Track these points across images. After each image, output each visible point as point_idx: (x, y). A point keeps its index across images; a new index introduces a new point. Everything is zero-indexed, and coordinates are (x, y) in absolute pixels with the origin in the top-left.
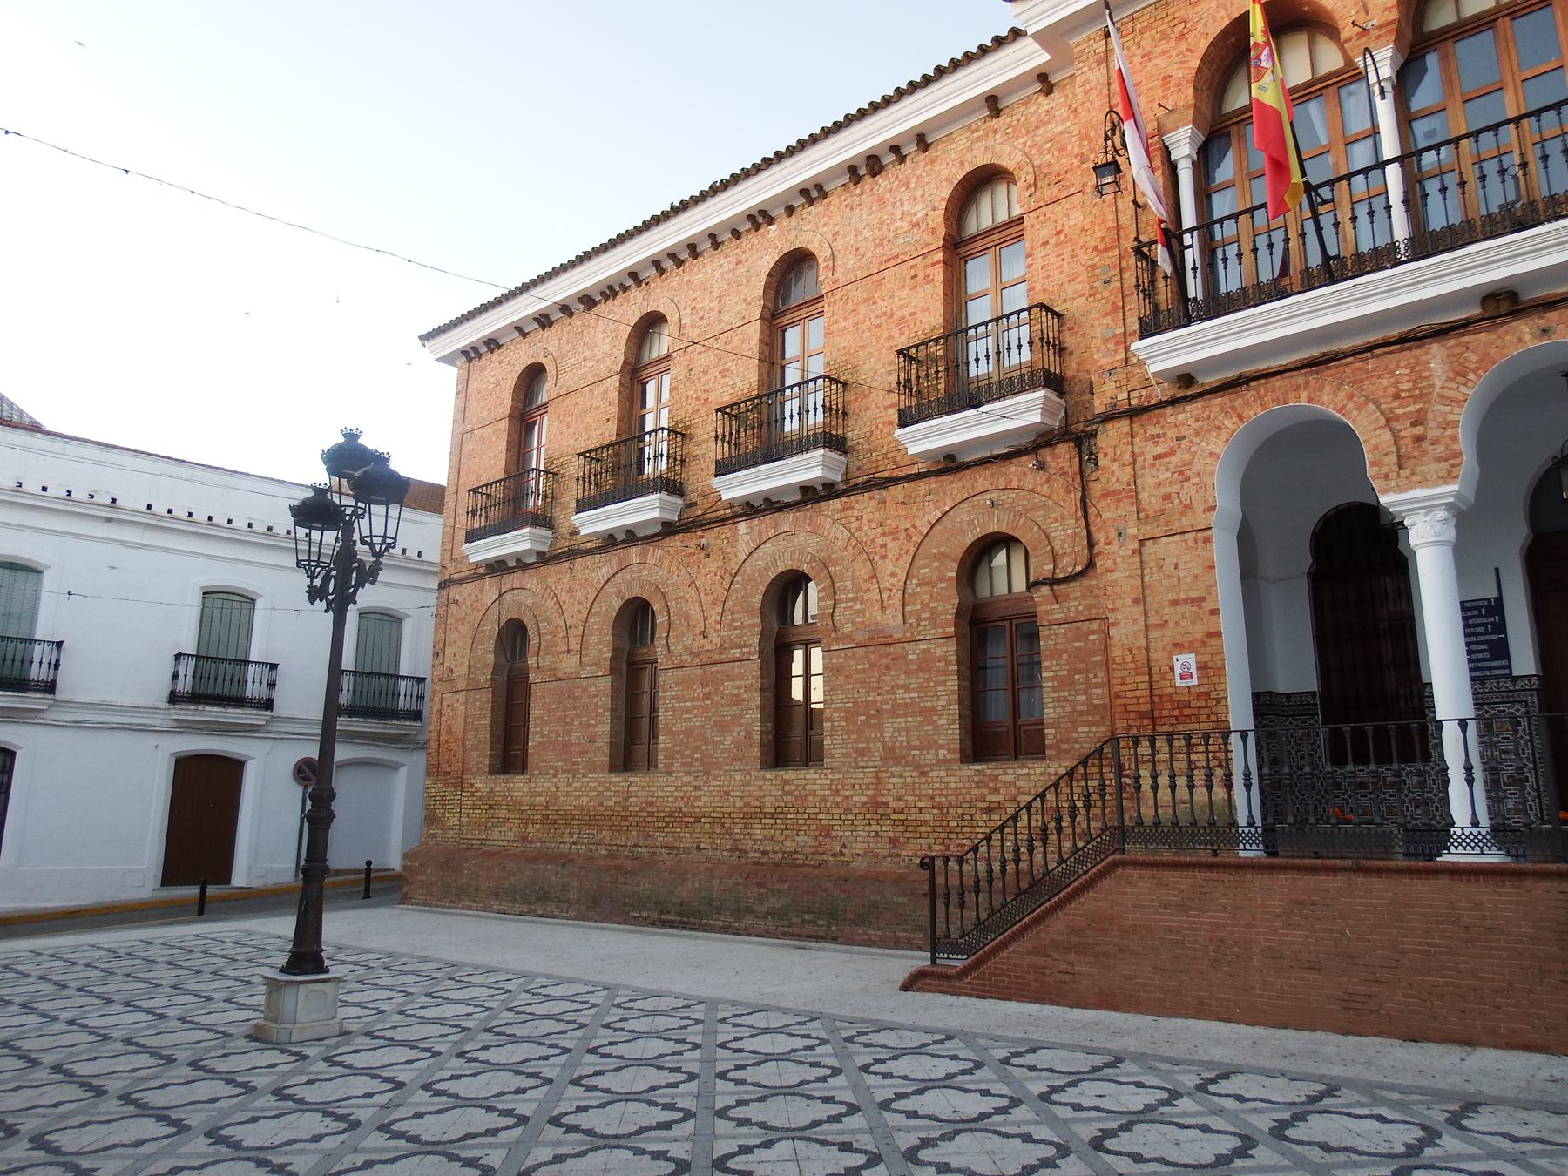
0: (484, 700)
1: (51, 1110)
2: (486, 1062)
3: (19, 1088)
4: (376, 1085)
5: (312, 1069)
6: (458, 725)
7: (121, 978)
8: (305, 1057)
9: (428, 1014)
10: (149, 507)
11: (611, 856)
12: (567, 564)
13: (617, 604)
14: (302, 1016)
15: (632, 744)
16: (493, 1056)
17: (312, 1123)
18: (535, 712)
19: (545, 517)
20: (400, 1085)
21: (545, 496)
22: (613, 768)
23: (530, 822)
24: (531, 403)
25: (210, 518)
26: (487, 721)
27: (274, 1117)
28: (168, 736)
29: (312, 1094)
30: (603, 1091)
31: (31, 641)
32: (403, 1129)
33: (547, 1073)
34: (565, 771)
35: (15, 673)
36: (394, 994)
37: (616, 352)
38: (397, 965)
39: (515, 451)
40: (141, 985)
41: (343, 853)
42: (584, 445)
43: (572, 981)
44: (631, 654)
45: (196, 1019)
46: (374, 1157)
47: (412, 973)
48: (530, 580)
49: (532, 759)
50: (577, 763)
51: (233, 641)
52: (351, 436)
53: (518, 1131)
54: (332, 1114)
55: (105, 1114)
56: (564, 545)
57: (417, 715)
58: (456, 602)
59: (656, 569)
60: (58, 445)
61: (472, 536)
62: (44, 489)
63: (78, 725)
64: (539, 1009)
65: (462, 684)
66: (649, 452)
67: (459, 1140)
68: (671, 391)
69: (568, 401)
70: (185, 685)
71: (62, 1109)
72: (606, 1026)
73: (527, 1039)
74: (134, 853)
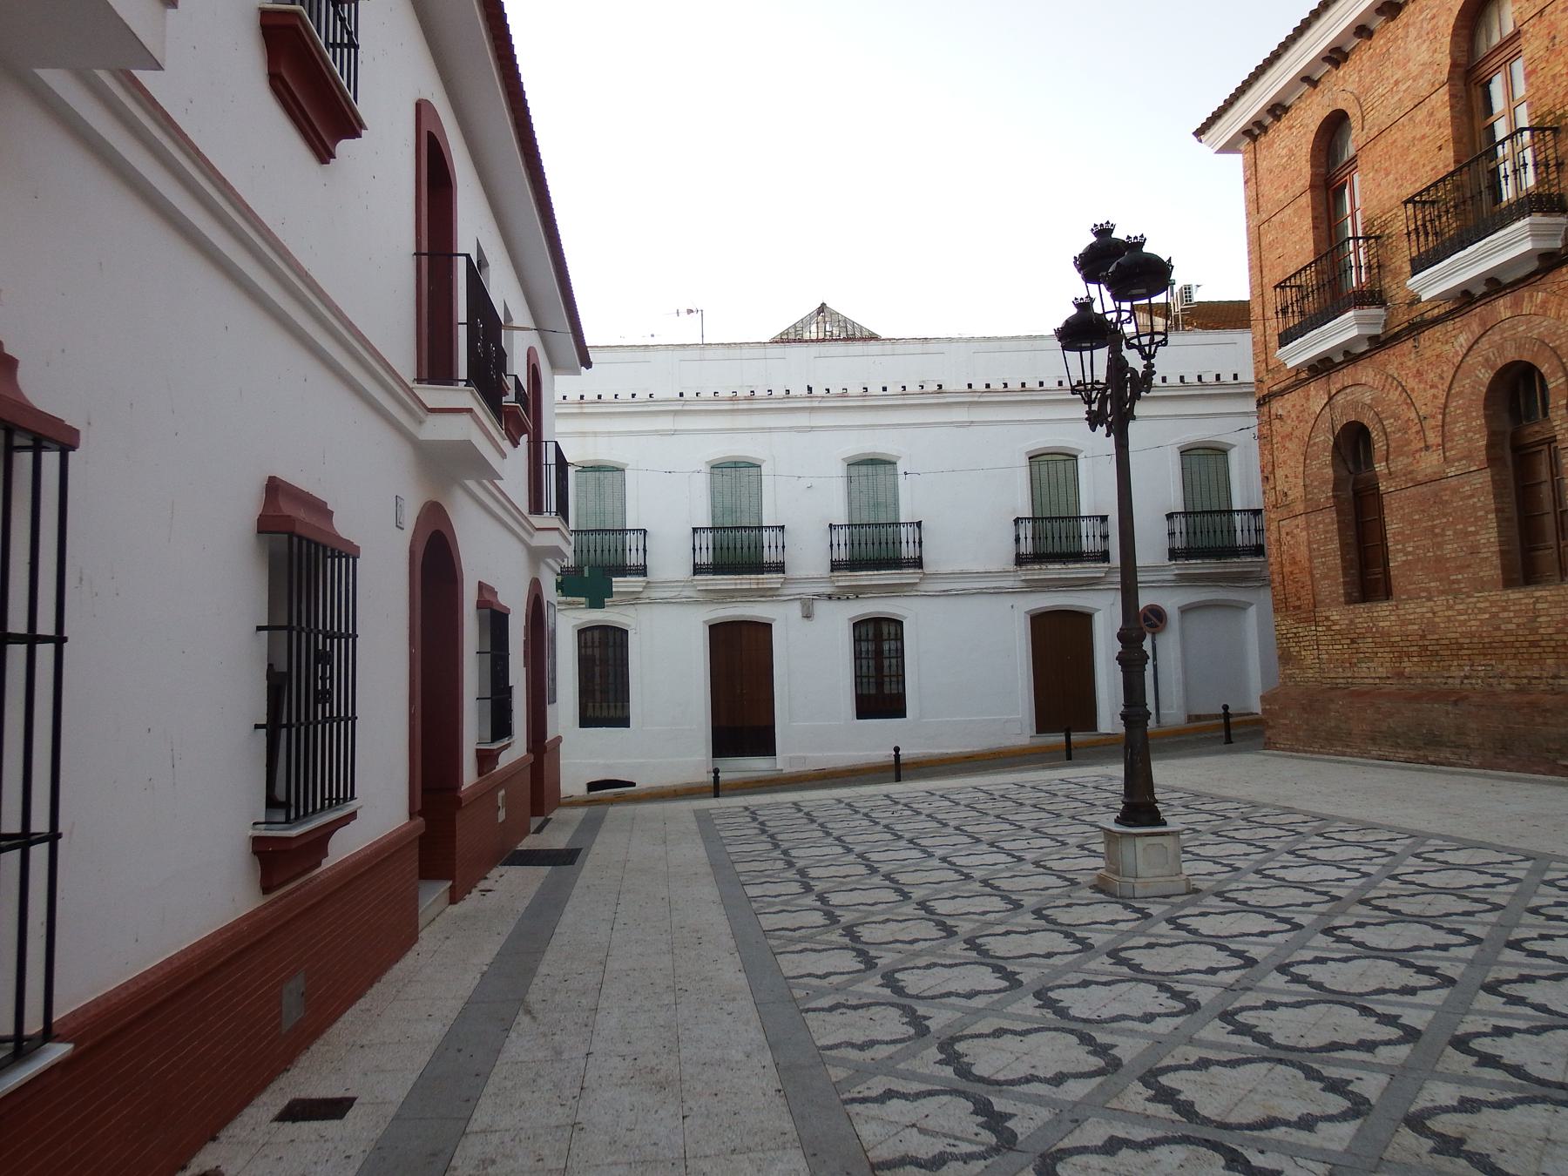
0: (1328, 521)
1: (908, 947)
2: (1361, 945)
3: (888, 920)
4: (1223, 959)
5: (1154, 930)
6: (1302, 553)
7: (991, 819)
8: (1147, 916)
9: (1291, 875)
10: (970, 386)
11: (1520, 690)
12: (1410, 343)
13: (1486, 376)
14: (1142, 869)
16: (1371, 936)
17: (1146, 997)
18: (1393, 527)
19: (1372, 293)
20: (1250, 962)
21: (1369, 268)
22: (1509, 583)
23: (1402, 655)
24: (1335, 164)
25: (1023, 385)
26: (1335, 545)
27: (1105, 984)
28: (1019, 596)
29: (1151, 961)
30: (1535, 1007)
31: (898, 524)
32: (1252, 1021)
33: (1447, 969)
34: (1443, 592)
35: (891, 554)
36: (1252, 849)
37: (1438, 56)
38: (1257, 816)
39: (1324, 226)
40: (1007, 826)
42: (1409, 190)
43: (1480, 846)
44: (1515, 436)
45: (1049, 864)
46: (1211, 1055)
47: (1274, 826)
48: (1366, 373)
49: (1398, 582)
50: (1458, 582)
51: (1063, 499)
52: (1103, 232)
53: (1404, 1051)
54: (1168, 989)
55: (951, 957)
56: (1403, 318)
57: (1259, 550)
58: (1280, 417)
59: (1537, 320)
60: (888, 347)
61: (1286, 338)
62: (885, 389)
63: (946, 594)
64: (1434, 880)
65: (1300, 508)
66: (1506, 168)
67: (1321, 1049)
68: (1528, 76)
69: (1382, 144)
70: (1027, 547)
71: (917, 946)
72: (1535, 911)
73: (1418, 919)
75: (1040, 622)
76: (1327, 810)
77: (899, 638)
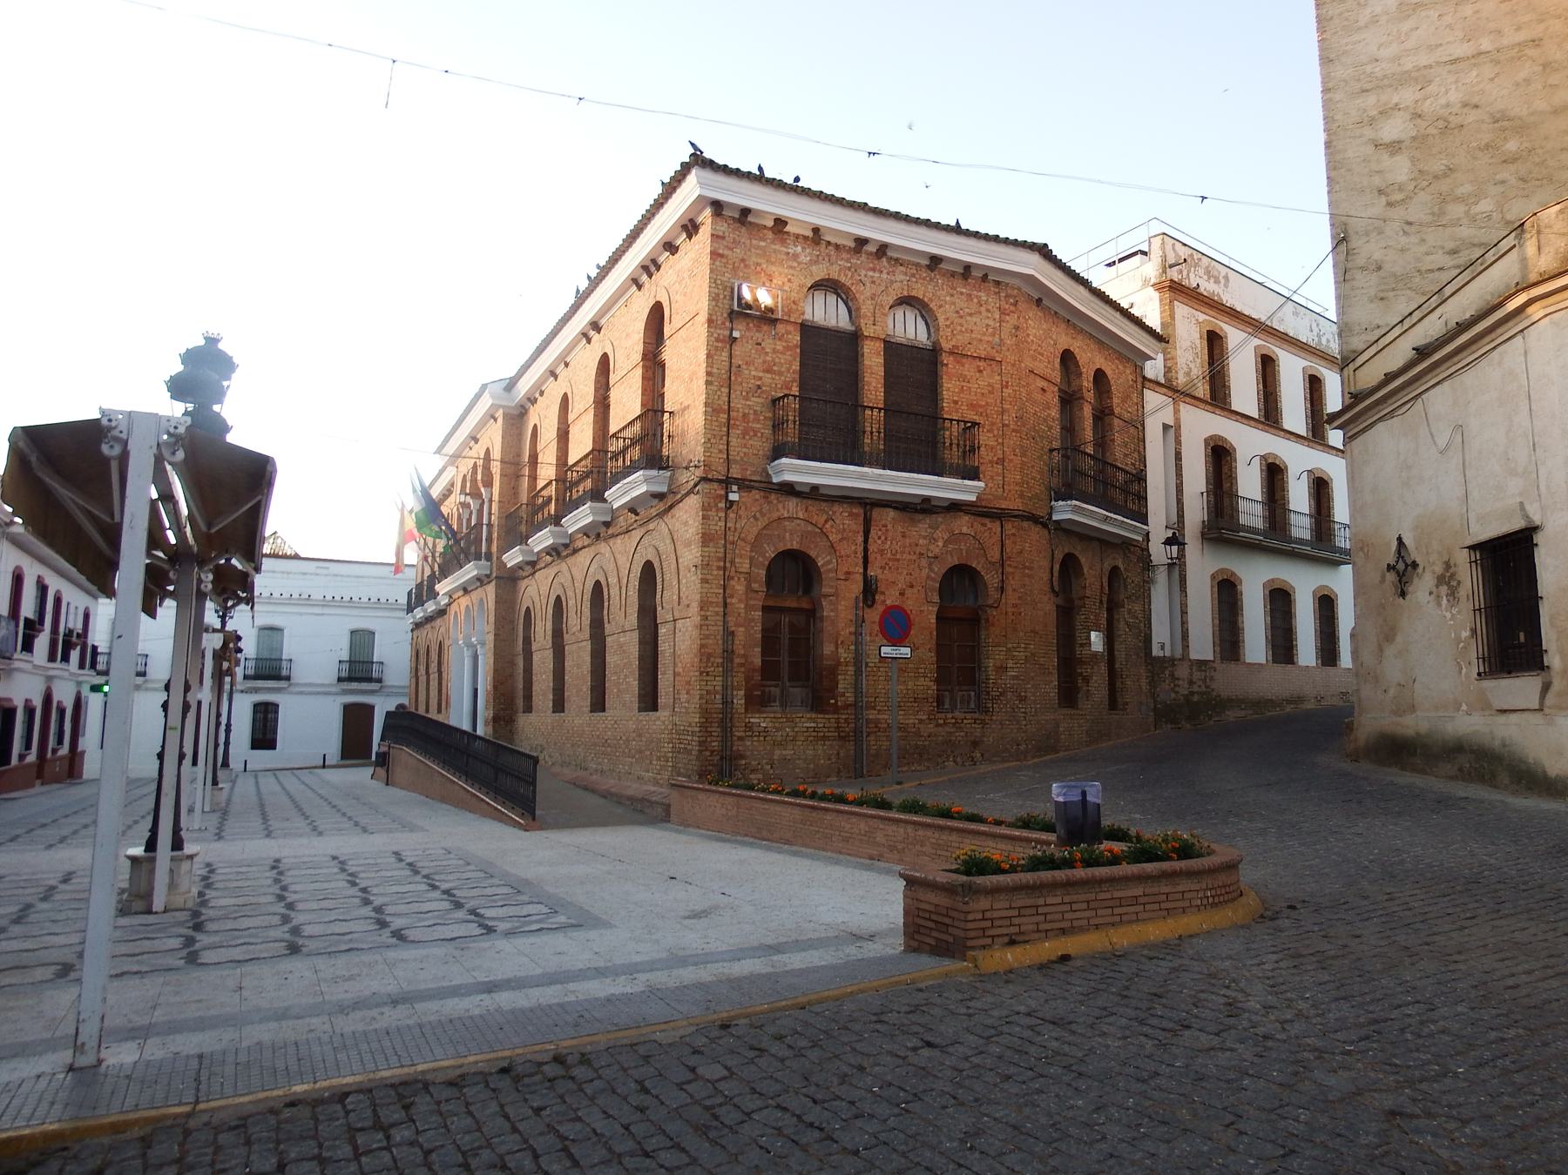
15: (599, 704)
41: (876, 513)
52: (212, 341)
63: (301, 693)
70: (344, 674)
74: (331, 743)
75: (349, 710)
76: (267, 841)
77: (277, 712)
